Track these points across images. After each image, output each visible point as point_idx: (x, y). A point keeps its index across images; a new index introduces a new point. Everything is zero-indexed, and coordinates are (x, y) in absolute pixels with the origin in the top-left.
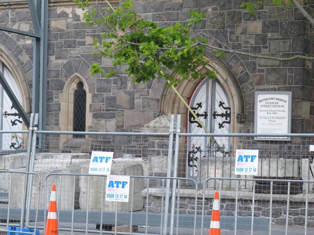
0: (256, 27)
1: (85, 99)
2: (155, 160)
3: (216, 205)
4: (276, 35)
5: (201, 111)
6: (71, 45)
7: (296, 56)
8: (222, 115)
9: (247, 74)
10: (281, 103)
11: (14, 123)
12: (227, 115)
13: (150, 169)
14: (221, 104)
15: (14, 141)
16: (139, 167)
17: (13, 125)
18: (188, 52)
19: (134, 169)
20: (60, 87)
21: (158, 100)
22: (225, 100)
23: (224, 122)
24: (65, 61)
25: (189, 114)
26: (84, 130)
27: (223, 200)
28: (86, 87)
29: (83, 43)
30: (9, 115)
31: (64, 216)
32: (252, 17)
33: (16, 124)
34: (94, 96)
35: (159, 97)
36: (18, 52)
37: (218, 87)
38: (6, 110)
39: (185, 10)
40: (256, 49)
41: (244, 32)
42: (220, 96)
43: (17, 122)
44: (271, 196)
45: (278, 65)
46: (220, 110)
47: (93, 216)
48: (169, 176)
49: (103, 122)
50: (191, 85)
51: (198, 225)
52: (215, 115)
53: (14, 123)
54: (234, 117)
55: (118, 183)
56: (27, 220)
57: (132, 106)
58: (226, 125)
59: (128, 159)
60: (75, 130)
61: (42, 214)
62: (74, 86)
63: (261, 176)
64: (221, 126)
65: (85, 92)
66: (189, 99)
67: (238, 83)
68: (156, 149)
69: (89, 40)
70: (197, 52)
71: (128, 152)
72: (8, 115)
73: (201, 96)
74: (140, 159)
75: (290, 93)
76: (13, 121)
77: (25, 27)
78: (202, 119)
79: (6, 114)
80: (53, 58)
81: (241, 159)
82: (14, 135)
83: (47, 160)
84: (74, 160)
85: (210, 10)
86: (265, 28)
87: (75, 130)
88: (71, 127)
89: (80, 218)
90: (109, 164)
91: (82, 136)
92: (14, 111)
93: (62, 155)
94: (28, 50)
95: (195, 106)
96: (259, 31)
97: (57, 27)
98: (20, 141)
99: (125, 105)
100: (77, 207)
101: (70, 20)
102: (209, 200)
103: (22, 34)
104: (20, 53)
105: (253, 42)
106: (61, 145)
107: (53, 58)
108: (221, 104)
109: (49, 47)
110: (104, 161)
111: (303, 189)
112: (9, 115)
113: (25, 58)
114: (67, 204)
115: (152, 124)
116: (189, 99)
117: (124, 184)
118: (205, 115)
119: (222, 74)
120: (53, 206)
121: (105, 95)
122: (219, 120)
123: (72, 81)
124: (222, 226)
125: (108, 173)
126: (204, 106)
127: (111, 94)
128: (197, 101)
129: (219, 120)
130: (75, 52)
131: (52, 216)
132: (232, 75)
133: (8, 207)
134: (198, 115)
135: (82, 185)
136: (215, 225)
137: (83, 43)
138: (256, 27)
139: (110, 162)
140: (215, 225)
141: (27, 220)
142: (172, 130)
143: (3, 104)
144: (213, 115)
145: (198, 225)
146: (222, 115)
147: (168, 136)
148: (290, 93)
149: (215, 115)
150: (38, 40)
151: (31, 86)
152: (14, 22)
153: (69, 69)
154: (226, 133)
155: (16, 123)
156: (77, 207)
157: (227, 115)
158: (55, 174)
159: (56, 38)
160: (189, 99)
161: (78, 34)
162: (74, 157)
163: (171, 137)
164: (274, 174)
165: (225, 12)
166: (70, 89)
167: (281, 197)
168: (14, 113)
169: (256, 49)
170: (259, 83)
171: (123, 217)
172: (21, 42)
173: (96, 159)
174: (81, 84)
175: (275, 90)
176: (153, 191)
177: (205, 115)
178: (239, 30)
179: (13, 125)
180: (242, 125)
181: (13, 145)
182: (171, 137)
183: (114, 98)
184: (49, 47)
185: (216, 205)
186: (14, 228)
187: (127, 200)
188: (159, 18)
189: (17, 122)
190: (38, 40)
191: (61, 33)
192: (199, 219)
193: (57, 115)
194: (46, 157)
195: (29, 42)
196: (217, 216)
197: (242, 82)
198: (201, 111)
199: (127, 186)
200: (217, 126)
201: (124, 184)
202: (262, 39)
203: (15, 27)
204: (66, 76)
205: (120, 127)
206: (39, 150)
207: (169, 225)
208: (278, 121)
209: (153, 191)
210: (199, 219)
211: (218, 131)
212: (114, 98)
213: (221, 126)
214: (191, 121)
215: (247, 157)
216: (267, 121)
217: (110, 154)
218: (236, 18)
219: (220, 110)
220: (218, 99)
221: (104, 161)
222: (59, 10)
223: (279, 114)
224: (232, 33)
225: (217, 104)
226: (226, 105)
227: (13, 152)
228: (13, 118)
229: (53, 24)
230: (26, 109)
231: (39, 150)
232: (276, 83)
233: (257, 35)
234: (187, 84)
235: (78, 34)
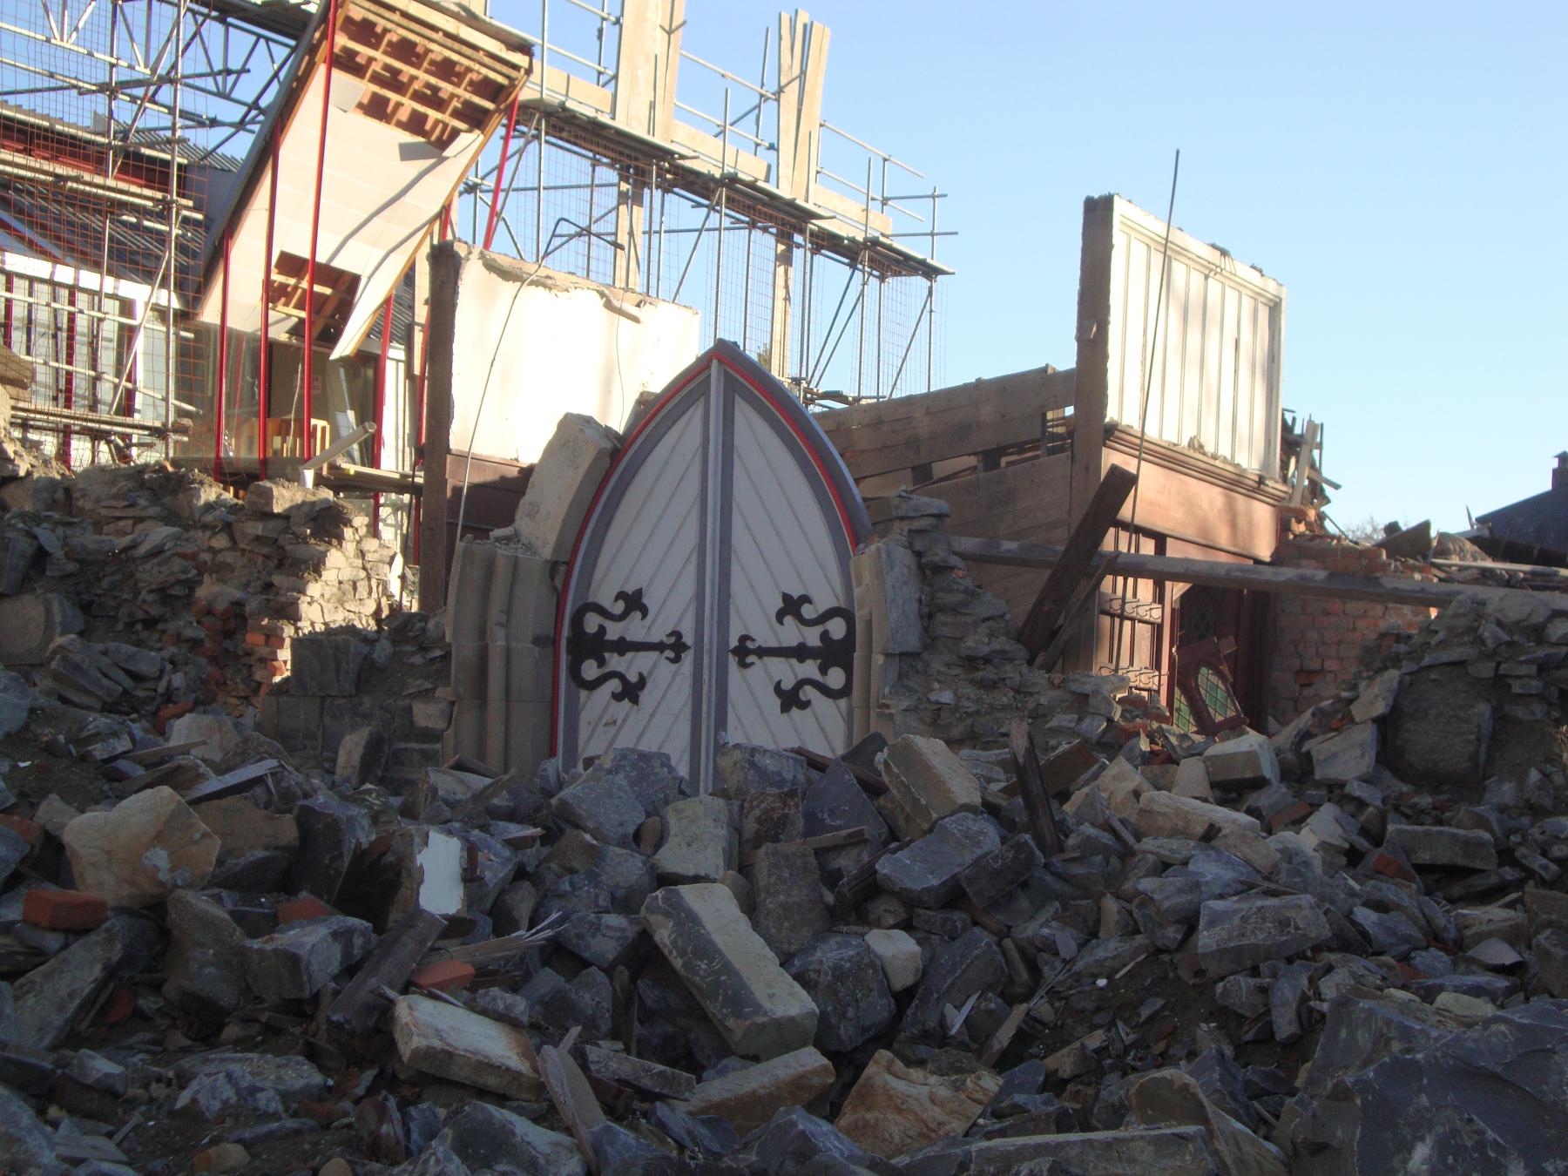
1: (568, 114)
11: (790, 699)
12: (835, 653)
17: (785, 708)
23: (622, 617)
25: (569, 641)
30: (763, 652)
33: (804, 705)
38: (746, 628)
43: (809, 693)
45: (526, 884)
53: (790, 699)
58: (605, 597)
63: (54, 268)
72: (760, 657)
76: (787, 685)
97: (570, 105)
111: (1389, 774)
112: (763, 652)
143: (728, 595)
144: (685, 647)
155: (802, 696)
168: (794, 643)
179: (785, 708)
189: (809, 693)
214: (593, 611)
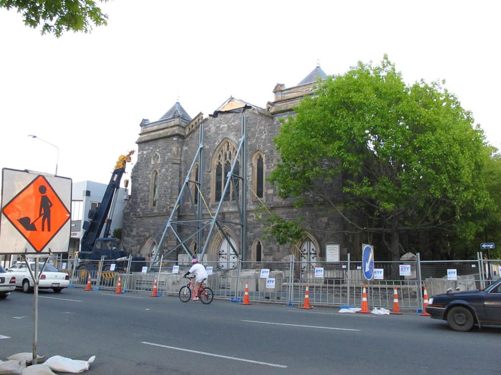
0: (325, 219)
2: (287, 271)
3: (307, 289)
4: (333, 223)
5: (305, 252)
6: (255, 228)
7: (339, 231)
8: (313, 254)
9: (322, 238)
10: (335, 249)
11: (234, 258)
12: (315, 254)
13: (285, 275)
14: (313, 249)
15: (234, 265)
16: (281, 275)
18: (298, 231)
19: (59, 255)
20: (251, 244)
21: (288, 248)
22: (314, 248)
24: (253, 234)
26: (261, 261)
27: (310, 287)
28: (261, 244)
29: (260, 227)
31: (251, 294)
32: (323, 216)
34: (264, 247)
35: (289, 247)
36: (235, 230)
37: (311, 243)
39: (298, 214)
40: (325, 228)
41: (321, 221)
42: (312, 246)
44: (334, 285)
46: (312, 252)
47: (262, 294)
48: (290, 278)
49: (268, 257)
50: (300, 243)
51: (301, 297)
52: (311, 254)
53: (234, 258)
54: (318, 255)
55: (271, 281)
56: (238, 295)
57: (279, 251)
58: (315, 258)
59: (277, 271)
60: (257, 261)
61: (243, 293)
62: (257, 243)
64: (313, 258)
65: (260, 246)
66: (300, 247)
67: (319, 241)
68: (287, 267)
69: (262, 226)
70: (302, 230)
71: (278, 269)
73: (305, 247)
74: (281, 272)
75: (339, 245)
77: (238, 221)
78: (306, 255)
79: (231, 254)
80: (248, 233)
81: (317, 271)
82: (234, 263)
83: (246, 272)
84: (256, 272)
85: (307, 214)
86: (329, 220)
87: (257, 261)
88: (256, 260)
89: (257, 295)
90: (268, 274)
91: (260, 263)
92: (234, 253)
93: (252, 270)
94: (239, 230)
95: (303, 250)
96: (326, 221)
98: (236, 265)
99: (276, 251)
100: (257, 290)
101: (254, 218)
102: (305, 287)
103: (236, 224)
104: (236, 231)
105: (324, 225)
106: (252, 267)
107: (248, 233)
108: (313, 249)
109: (247, 228)
110: (379, 273)
113: (238, 233)
114: (253, 289)
115: (285, 258)
116: (300, 248)
117: (273, 281)
118: (307, 254)
119: (312, 238)
120: (247, 290)
121: (269, 247)
122: (312, 256)
123: (256, 241)
124: (309, 297)
125: (267, 277)
126: (306, 250)
127: (271, 246)
128: (304, 248)
129: (312, 256)
130: (257, 230)
131: (246, 293)
132: (317, 238)
133: (230, 290)
134: (304, 254)
135: (259, 282)
136: (307, 296)
137: (260, 227)
138: (325, 219)
139: (268, 273)
140: (307, 296)
141: (238, 295)
142: (291, 261)
145: (301, 297)
146: (313, 254)
147: (290, 263)
148: (339, 245)
149: (311, 254)
150: (243, 226)
151: (240, 243)
152: (233, 219)
153: (255, 237)
154: (315, 261)
156: (257, 290)
157: (315, 254)
158: (249, 277)
159: (249, 225)
160: (300, 248)
161: (258, 223)
162: (257, 271)
163: (291, 263)
164: (329, 277)
165: (313, 214)
166: (255, 244)
167: (331, 285)
169: (325, 228)
170: (327, 241)
171: (273, 294)
172: (236, 227)
173: (263, 272)
174: (259, 243)
175: (333, 244)
176: (285, 284)
177: (307, 254)
178: (319, 221)
180: (321, 258)
181: (234, 266)
182: (291, 263)
183: (272, 248)
184: (247, 228)
185: (307, 289)
186: (232, 298)
187: (274, 287)
188: (288, 217)
190: (243, 226)
191: (252, 223)
192: (301, 294)
193: (250, 255)
194: (246, 271)
195: (239, 227)
196: (307, 292)
197: (321, 241)
198: (305, 252)
199: (274, 282)
200: (312, 258)
201: (273, 281)
202: (328, 224)
203: (234, 221)
204: (254, 240)
205: (274, 259)
206: (242, 268)
207: (291, 297)
208: (335, 256)
209: (285, 284)
210: (301, 294)
211: (312, 260)
212: (272, 248)
213: (313, 258)
215: (265, 272)
216: (330, 256)
217: (269, 270)
218: (317, 216)
219: (312, 252)
220: (312, 248)
221: (379, 273)
222: (251, 214)
223: (336, 253)
224: (316, 222)
225: (311, 250)
226: (315, 250)
227: (233, 269)
228: (234, 256)
229: (248, 220)
230: (238, 253)
231: (242, 268)
232: (333, 241)
233: (326, 223)
234: (299, 243)
235: (258, 223)
